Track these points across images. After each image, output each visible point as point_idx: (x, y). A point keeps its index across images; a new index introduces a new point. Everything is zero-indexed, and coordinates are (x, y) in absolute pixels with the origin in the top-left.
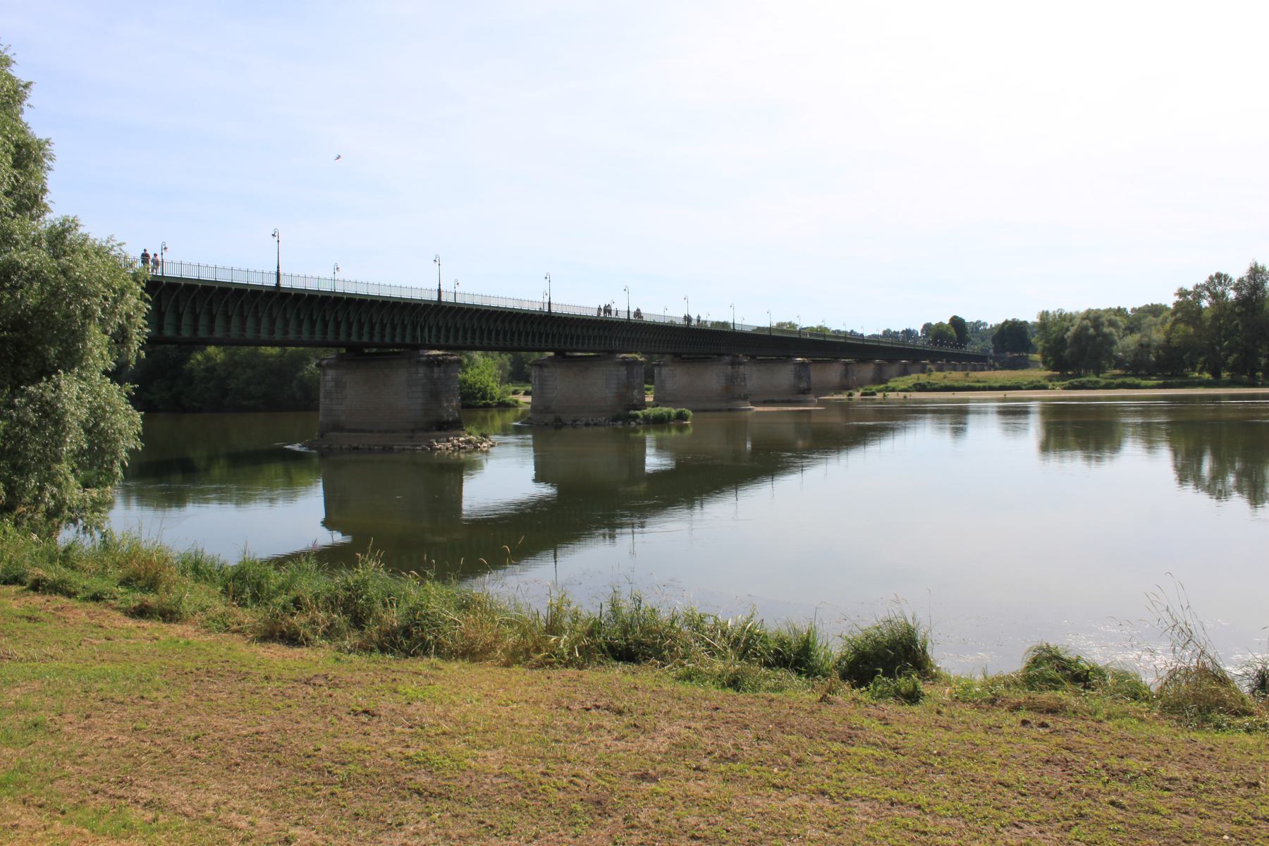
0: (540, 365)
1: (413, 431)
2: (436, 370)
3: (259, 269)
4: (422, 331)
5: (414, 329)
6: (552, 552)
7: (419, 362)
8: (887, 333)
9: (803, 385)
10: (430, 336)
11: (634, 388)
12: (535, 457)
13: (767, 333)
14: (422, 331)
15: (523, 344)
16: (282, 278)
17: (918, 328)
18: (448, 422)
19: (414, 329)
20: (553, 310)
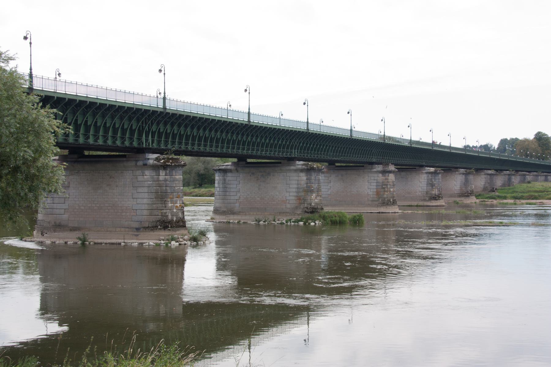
0: (224, 171)
1: (138, 229)
2: (162, 173)
3: (95, 84)
4: (147, 136)
5: (140, 135)
6: (246, 342)
7: (145, 165)
8: (466, 147)
9: (435, 192)
10: (147, 140)
11: (312, 192)
12: (182, 278)
13: (406, 144)
14: (147, 136)
15: (190, 148)
16: (34, 80)
17: (495, 144)
18: (171, 222)
19: (140, 135)
20: (386, 134)
